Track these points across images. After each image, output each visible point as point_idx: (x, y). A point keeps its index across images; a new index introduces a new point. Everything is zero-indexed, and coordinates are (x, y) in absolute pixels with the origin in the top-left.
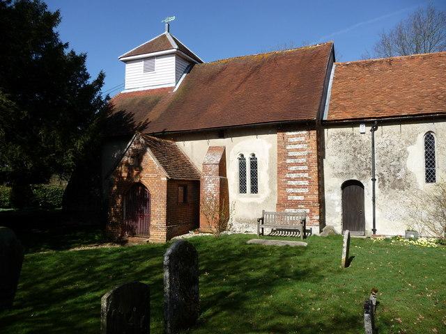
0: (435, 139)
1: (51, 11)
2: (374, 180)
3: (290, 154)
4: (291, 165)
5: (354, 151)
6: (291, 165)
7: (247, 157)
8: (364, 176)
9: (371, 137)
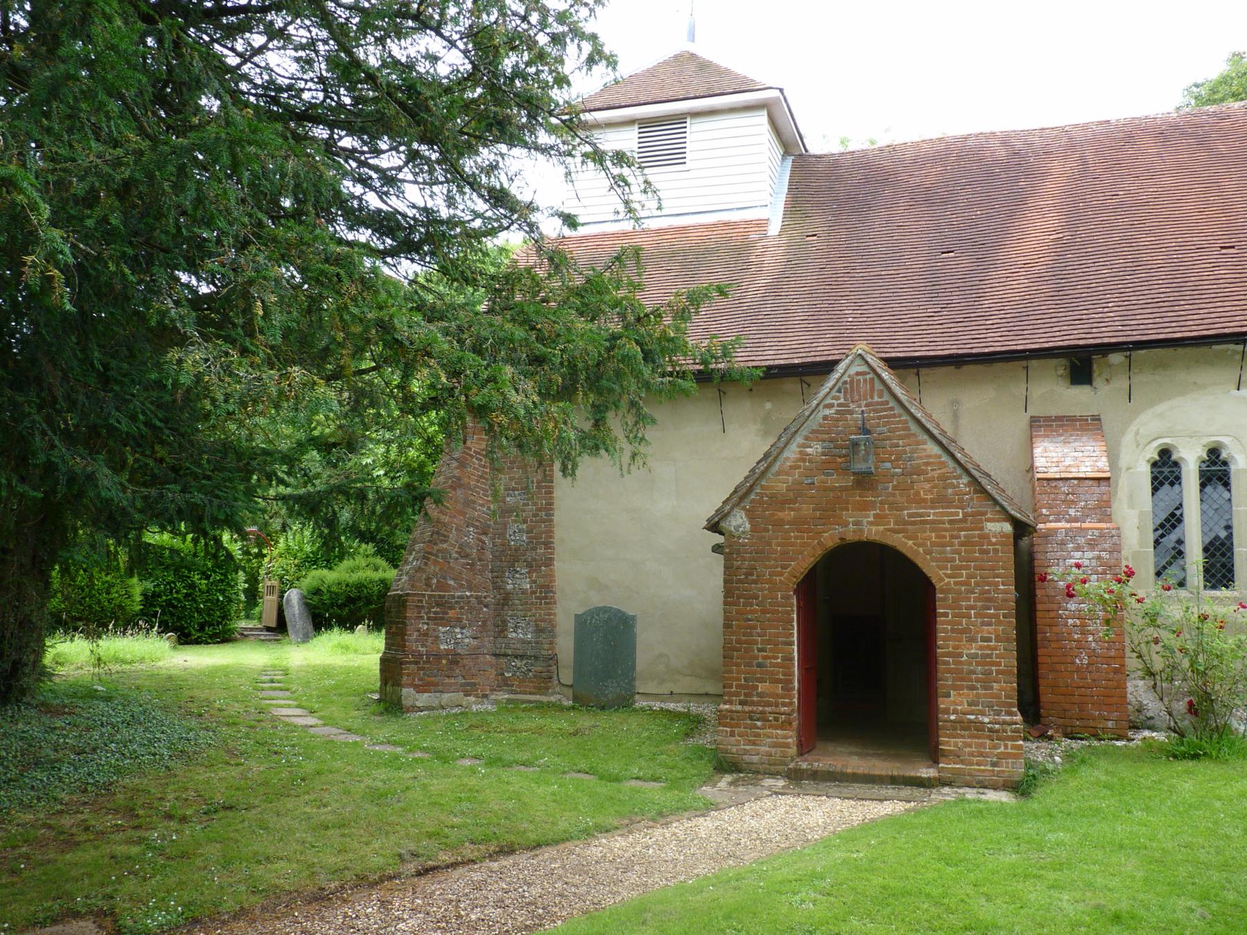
7: (1191, 459)
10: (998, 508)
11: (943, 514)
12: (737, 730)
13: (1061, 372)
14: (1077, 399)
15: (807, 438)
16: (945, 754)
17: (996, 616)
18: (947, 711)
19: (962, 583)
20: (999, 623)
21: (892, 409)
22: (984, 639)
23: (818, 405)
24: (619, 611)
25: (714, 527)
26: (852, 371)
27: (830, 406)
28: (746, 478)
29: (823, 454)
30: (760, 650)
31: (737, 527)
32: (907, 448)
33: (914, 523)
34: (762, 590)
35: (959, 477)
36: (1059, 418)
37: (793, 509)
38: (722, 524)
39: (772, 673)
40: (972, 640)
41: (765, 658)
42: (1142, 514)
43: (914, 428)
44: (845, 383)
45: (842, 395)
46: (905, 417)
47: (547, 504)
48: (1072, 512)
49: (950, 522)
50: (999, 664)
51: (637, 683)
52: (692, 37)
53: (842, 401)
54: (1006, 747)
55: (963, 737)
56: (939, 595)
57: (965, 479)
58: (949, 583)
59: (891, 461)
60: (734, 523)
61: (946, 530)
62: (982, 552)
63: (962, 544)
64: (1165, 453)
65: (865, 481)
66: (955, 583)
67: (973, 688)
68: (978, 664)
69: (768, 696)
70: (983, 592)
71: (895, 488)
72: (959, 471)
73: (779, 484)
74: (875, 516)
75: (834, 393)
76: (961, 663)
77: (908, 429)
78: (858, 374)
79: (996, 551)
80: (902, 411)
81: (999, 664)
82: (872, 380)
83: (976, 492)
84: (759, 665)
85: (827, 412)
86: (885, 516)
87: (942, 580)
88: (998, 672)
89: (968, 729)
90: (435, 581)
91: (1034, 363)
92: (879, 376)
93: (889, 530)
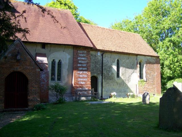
0: (120, 61)
1: (22, 28)
2: (102, 76)
3: (80, 62)
4: (80, 67)
5: (95, 63)
6: (80, 67)
7: (57, 61)
8: (99, 74)
9: (102, 58)
10: (38, 67)
11: (30, 67)
14: (43, 51)
15: (8, 53)
16: (29, 106)
18: (29, 99)
21: (23, 50)
26: (17, 42)
27: (13, 48)
35: (33, 62)
36: (40, 53)
40: (34, 87)
42: (50, 69)
46: (25, 51)
49: (31, 69)
50: (37, 91)
51: (124, 69)
56: (29, 81)
57: (34, 62)
64: (54, 60)
65: (18, 61)
67: (33, 95)
72: (33, 61)
78: (18, 43)
83: (35, 64)
85: (13, 49)
87: (29, 78)
92: (21, 44)
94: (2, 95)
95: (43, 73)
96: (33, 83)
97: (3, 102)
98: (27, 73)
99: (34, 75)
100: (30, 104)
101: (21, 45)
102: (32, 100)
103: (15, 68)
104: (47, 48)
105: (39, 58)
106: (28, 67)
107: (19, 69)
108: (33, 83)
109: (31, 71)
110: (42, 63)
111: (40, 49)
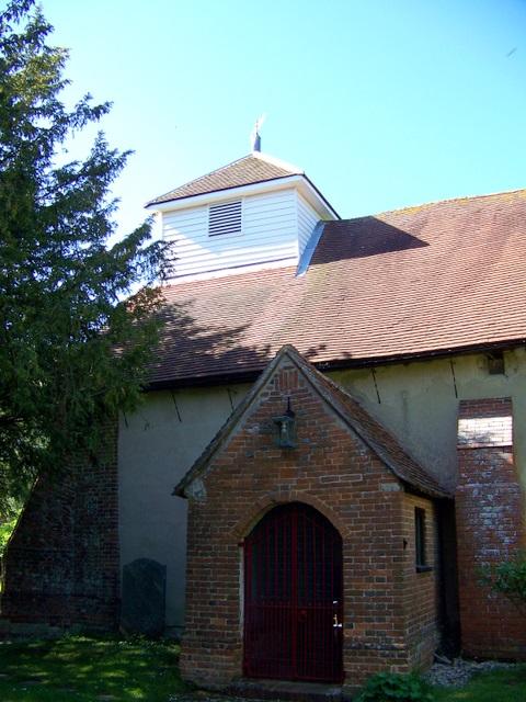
12: (193, 655)
13: (481, 365)
14: (494, 386)
17: (387, 560)
18: (349, 640)
19: (362, 534)
20: (390, 566)
21: (310, 395)
22: (379, 580)
23: (256, 394)
24: (153, 561)
25: (180, 492)
26: (281, 366)
27: (265, 395)
28: (204, 454)
29: (260, 433)
30: (213, 591)
31: (197, 494)
32: (322, 426)
33: (326, 486)
34: (214, 543)
35: (361, 447)
36: (480, 401)
37: (236, 478)
38: (186, 491)
39: (221, 610)
40: (370, 580)
41: (216, 597)
43: (326, 409)
44: (276, 376)
45: (274, 386)
46: (320, 401)
47: (114, 481)
48: (484, 474)
52: (258, 147)
53: (274, 390)
54: (355, 668)
55: (361, 661)
58: (352, 535)
59: (309, 436)
60: (195, 490)
61: (349, 491)
62: (377, 507)
63: (363, 502)
66: (358, 534)
68: (374, 600)
69: (216, 627)
70: (378, 540)
71: (312, 457)
72: (360, 442)
73: (224, 457)
74: (298, 481)
75: (268, 384)
76: (359, 600)
77: (322, 410)
78: (286, 368)
79: (388, 506)
80: (318, 396)
81: (390, 600)
82: (296, 372)
84: (211, 603)
86: (305, 481)
87: (346, 532)
88: (390, 607)
89: (365, 654)
90: (29, 539)
91: (460, 359)
93: (309, 492)
94: (226, 616)
95: (490, 497)
96: (367, 554)
97: (226, 645)
98: (337, 509)
99: (372, 514)
100: (350, 666)
101: (300, 377)
102: (361, 649)
103: (279, 485)
104: (516, 370)
105: (470, 427)
106: (337, 479)
107: (296, 493)
108: (367, 554)
109: (355, 496)
110: (485, 449)
111: (475, 381)
